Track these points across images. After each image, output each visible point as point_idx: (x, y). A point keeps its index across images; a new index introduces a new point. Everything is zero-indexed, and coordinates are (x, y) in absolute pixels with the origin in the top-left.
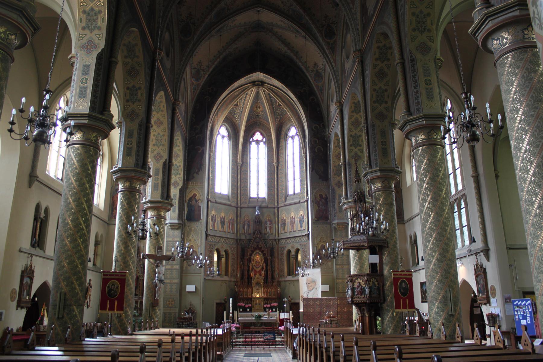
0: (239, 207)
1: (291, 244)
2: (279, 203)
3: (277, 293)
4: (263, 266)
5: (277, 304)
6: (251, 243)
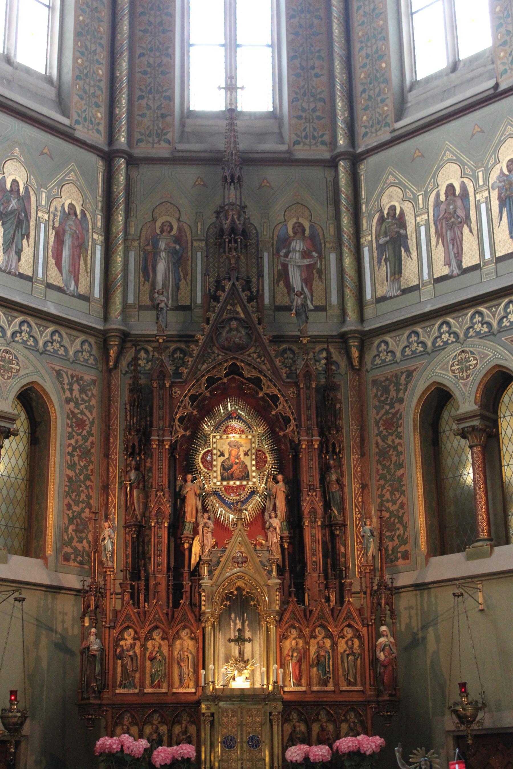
0: (121, 153)
1: (454, 350)
2: (360, 130)
3: (374, 661)
4: (269, 496)
5: (379, 740)
6: (195, 350)
